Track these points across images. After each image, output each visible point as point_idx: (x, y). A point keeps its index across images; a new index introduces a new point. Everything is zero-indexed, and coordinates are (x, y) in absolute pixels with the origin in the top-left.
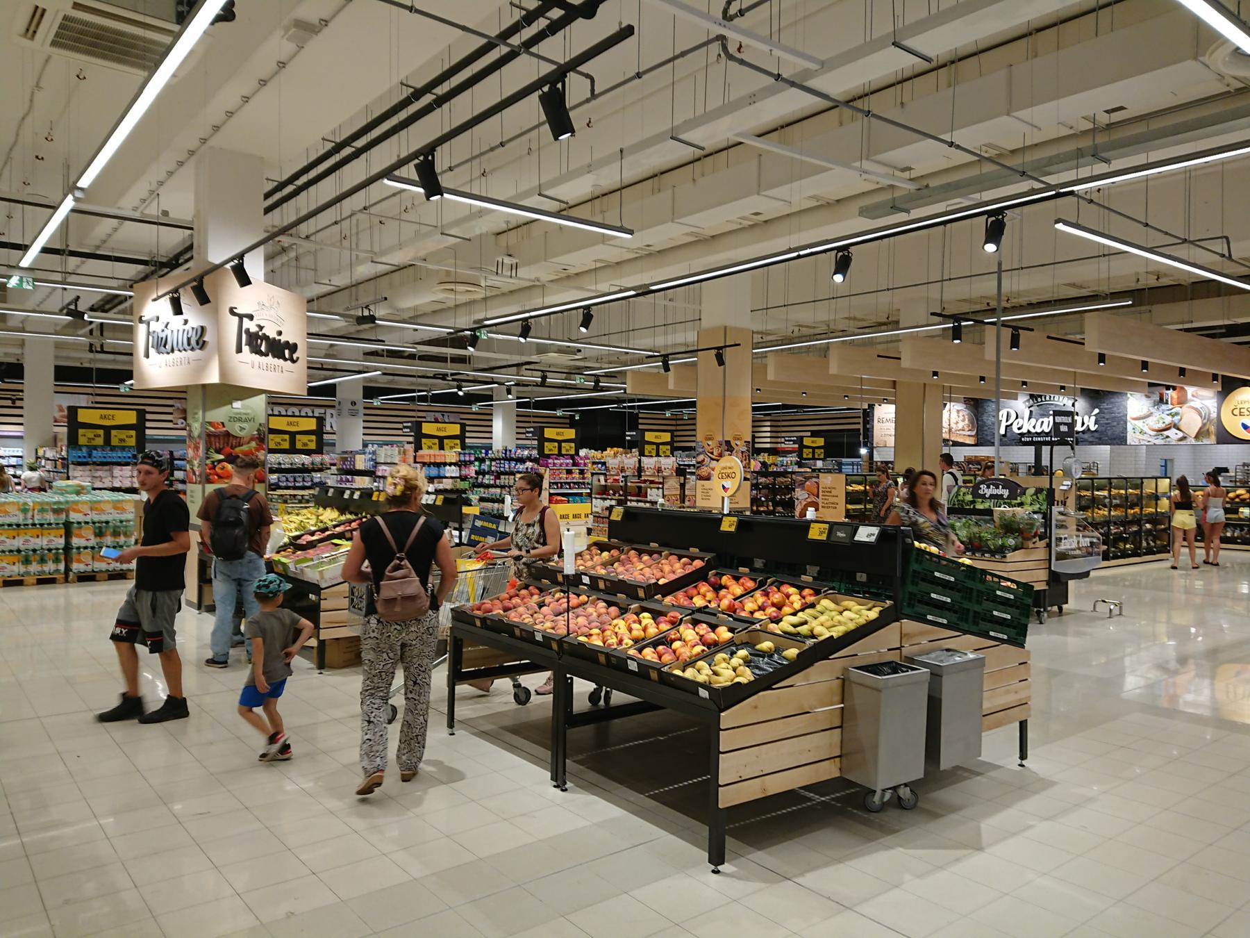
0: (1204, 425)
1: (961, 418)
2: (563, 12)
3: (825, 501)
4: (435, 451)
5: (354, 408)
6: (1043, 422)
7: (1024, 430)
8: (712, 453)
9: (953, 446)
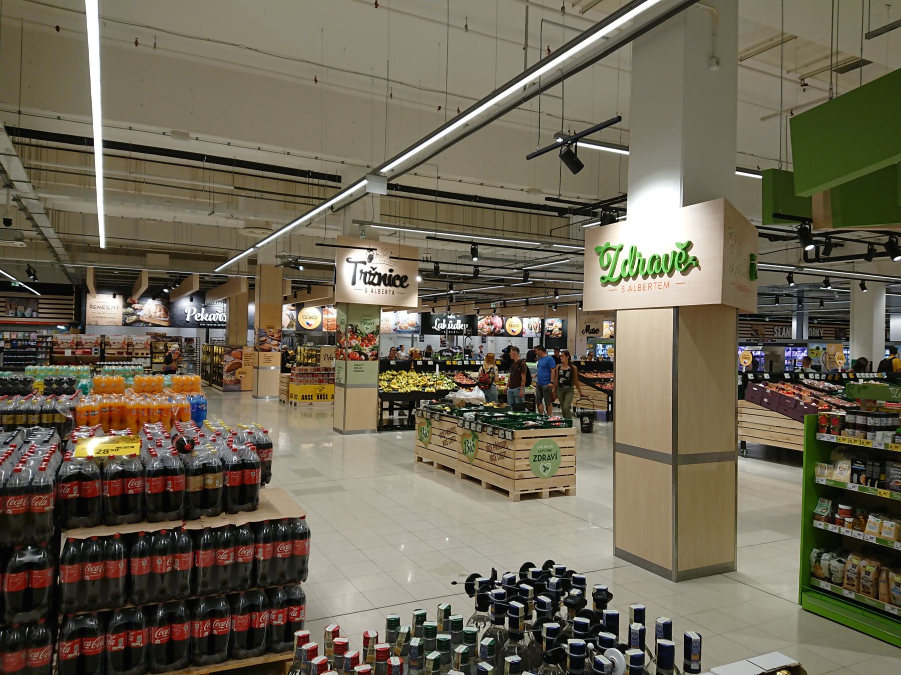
0: (291, 322)
2: (493, 639)
4: (135, 339)
7: (202, 319)
8: (273, 336)
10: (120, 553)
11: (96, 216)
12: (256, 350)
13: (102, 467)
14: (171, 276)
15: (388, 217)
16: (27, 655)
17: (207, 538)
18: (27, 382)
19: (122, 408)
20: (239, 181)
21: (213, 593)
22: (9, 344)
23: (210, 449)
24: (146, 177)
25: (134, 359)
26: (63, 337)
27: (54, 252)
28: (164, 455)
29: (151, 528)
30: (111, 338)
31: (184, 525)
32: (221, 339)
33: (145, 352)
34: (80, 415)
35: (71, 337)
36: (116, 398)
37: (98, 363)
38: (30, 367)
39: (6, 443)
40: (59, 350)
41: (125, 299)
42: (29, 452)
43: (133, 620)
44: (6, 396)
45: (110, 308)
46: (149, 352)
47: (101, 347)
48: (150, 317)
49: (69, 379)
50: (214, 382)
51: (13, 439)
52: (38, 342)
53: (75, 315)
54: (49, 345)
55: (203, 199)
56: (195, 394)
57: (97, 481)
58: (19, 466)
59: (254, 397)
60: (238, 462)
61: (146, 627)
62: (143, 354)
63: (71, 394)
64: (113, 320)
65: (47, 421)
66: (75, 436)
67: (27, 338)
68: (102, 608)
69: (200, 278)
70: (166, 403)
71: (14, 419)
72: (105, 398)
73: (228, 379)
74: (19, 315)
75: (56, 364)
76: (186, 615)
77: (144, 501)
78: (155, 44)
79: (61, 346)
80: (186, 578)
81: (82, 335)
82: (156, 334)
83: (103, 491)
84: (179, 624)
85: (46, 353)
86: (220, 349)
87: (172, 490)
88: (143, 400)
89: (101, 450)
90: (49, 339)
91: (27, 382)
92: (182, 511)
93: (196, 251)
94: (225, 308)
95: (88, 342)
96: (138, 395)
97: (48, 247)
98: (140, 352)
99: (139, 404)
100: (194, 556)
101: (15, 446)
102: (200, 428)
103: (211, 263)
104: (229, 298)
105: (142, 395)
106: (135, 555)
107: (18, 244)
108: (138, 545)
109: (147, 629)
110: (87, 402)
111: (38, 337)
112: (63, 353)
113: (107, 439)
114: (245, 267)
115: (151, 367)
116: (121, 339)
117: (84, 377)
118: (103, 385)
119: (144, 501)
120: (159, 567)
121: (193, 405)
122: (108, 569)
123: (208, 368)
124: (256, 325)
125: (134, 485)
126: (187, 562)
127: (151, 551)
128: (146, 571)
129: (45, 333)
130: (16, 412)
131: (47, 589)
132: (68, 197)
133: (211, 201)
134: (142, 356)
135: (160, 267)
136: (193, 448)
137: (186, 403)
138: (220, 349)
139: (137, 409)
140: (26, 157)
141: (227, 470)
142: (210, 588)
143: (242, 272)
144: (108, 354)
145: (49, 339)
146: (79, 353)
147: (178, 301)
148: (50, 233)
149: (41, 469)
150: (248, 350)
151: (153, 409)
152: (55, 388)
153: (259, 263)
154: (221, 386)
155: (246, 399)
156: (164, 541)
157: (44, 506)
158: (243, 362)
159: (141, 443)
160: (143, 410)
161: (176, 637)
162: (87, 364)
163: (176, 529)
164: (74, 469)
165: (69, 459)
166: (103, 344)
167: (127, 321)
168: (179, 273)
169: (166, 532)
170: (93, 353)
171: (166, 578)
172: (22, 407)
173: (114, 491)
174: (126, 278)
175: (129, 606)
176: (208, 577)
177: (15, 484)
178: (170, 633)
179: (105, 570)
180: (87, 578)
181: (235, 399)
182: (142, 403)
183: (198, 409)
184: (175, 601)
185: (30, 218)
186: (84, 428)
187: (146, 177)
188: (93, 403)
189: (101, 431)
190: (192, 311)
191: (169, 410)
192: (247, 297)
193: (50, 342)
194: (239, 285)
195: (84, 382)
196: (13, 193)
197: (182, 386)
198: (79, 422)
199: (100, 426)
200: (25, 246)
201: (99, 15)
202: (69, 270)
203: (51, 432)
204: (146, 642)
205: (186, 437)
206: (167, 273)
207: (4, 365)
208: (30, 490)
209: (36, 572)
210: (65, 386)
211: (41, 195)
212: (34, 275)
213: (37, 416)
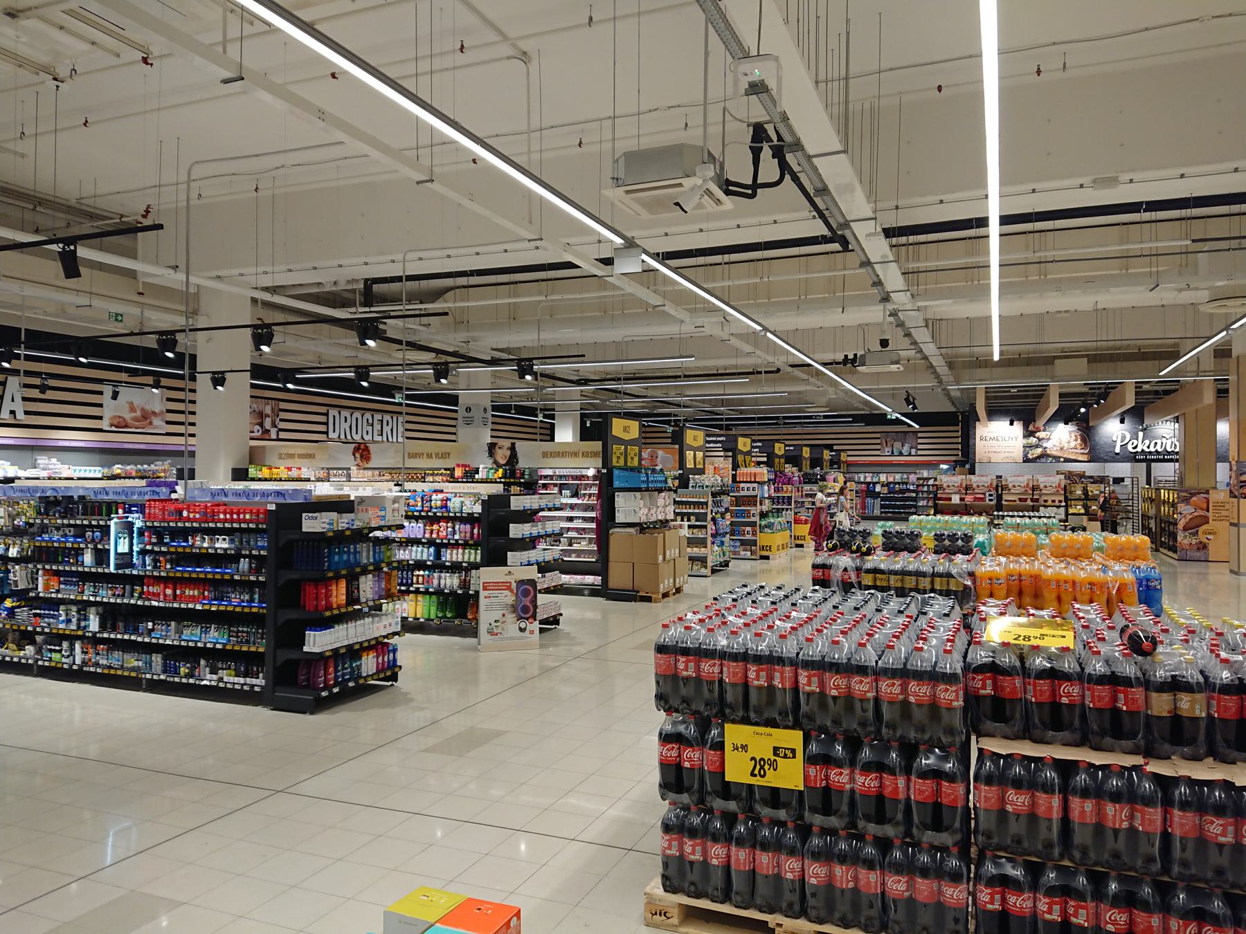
1: (1074, 438)
3: (1217, 515)
4: (1042, 480)
5: (469, 415)
6: (1156, 443)
7: (1139, 449)
9: (1064, 462)
10: (1053, 785)
11: (990, 317)
12: (1232, 494)
13: (1022, 658)
14: (1090, 389)
15: (1149, 258)
16: (940, 888)
17: (1185, 792)
18: (914, 536)
19: (1036, 578)
20: (1198, 229)
21: (1199, 880)
22: (886, 488)
23: (1182, 655)
24: (1159, 245)
25: (1041, 508)
26: (950, 480)
27: (935, 372)
28: (1110, 654)
29: (1098, 759)
30: (1010, 479)
31: (1147, 764)
32: (1172, 479)
33: (1057, 498)
34: (981, 583)
35: (958, 479)
36: (1027, 563)
37: (996, 513)
38: (914, 516)
39: (901, 612)
40: (944, 496)
41: (1026, 427)
42: (928, 626)
43: (1073, 885)
44: (892, 552)
45: (1007, 439)
46: (1062, 498)
47: (997, 491)
48: (1062, 449)
49: (964, 534)
50: (1163, 545)
51: (907, 607)
52: (918, 486)
53: (962, 450)
54: (931, 489)
55: (1139, 268)
56: (1143, 565)
57: (1017, 677)
58: (919, 643)
59: (1231, 571)
60: (1232, 680)
61: (1092, 901)
62: (1054, 501)
63: (968, 554)
64: (1011, 455)
65: (941, 587)
66: (982, 611)
67: (906, 480)
68: (1029, 855)
69: (1136, 387)
70: (1099, 576)
71: (902, 581)
72: (1012, 562)
73: (1186, 542)
74: (896, 454)
75: (943, 513)
76: (1154, 902)
77: (1083, 716)
78: (1065, 63)
79: (947, 491)
80: (1153, 846)
81: (972, 476)
82: (1070, 472)
83: (1025, 693)
84: (1143, 912)
85: (929, 499)
86: (1171, 495)
87: (1125, 708)
88: (1065, 568)
89: (1020, 636)
90: (931, 482)
91: (914, 536)
92: (1142, 743)
93: (1128, 347)
94: (1177, 431)
95: (980, 485)
96: (1057, 561)
97: (928, 367)
98: (1050, 499)
99: (1059, 574)
100: (1165, 816)
101: (911, 617)
102: (1157, 616)
103: (1150, 363)
104: (1184, 414)
105: (1062, 561)
106: (1074, 792)
107: (894, 367)
108: (1078, 778)
109: (1094, 904)
110: (990, 566)
111: (918, 479)
112: (950, 499)
113: (1023, 620)
114: (1209, 363)
115: (1066, 521)
116: (1023, 480)
117: (980, 532)
118: (1008, 544)
119: (1083, 716)
120: (1111, 817)
121: (1140, 582)
122: (1037, 803)
123: (1152, 524)
124: (1233, 454)
125: (1069, 692)
126: (1154, 821)
127: (1096, 792)
128: (1091, 819)
129: (925, 474)
130: (904, 573)
131: (959, 809)
132: (950, 301)
133: (1153, 269)
134: (1053, 504)
135: (1075, 377)
136: (1155, 649)
137: (1129, 577)
138: (1171, 495)
139: (1058, 581)
140: (903, 260)
141: (1214, 692)
142: (1193, 871)
143: (1205, 371)
144: (1006, 501)
145: (931, 482)
146: (969, 499)
147: (1101, 423)
148: (930, 349)
149: (946, 651)
150: (1219, 496)
151: (1080, 583)
152: (950, 545)
153: (1234, 354)
154: (1175, 552)
155: (1218, 575)
156: (1117, 782)
157: (951, 701)
158: (1210, 515)
159: (1075, 632)
160: (1066, 582)
161: (887, 792)
162: (980, 514)
163: (1134, 768)
164: (986, 657)
165: (979, 643)
166: (1000, 489)
167: (1030, 456)
168: (1105, 383)
169: (1118, 768)
170: (987, 500)
171: (1122, 837)
172: (911, 568)
173: (1041, 695)
174: (1026, 397)
175: (1066, 863)
176: (1189, 855)
177: (917, 665)
178: (1130, 920)
179: (1033, 804)
180: (1009, 808)
181: (1199, 574)
182: (1064, 572)
183: (1147, 586)
184: (1135, 874)
185: (908, 335)
186: (992, 601)
187: (1159, 245)
188: (997, 568)
189: (1012, 608)
190: (1124, 438)
191: (1103, 586)
192: (1214, 410)
193: (933, 485)
194: (1200, 394)
195: (980, 538)
196: (890, 307)
197: (1121, 550)
198: (981, 592)
199: (1013, 601)
200: (902, 369)
201: (998, 50)
202: (952, 393)
203: (951, 602)
204: (1093, 922)
205: (1142, 631)
206: (1085, 384)
207: (882, 512)
208: (934, 676)
209: (946, 784)
210: (960, 543)
211: (920, 304)
212: (914, 403)
213: (928, 580)
